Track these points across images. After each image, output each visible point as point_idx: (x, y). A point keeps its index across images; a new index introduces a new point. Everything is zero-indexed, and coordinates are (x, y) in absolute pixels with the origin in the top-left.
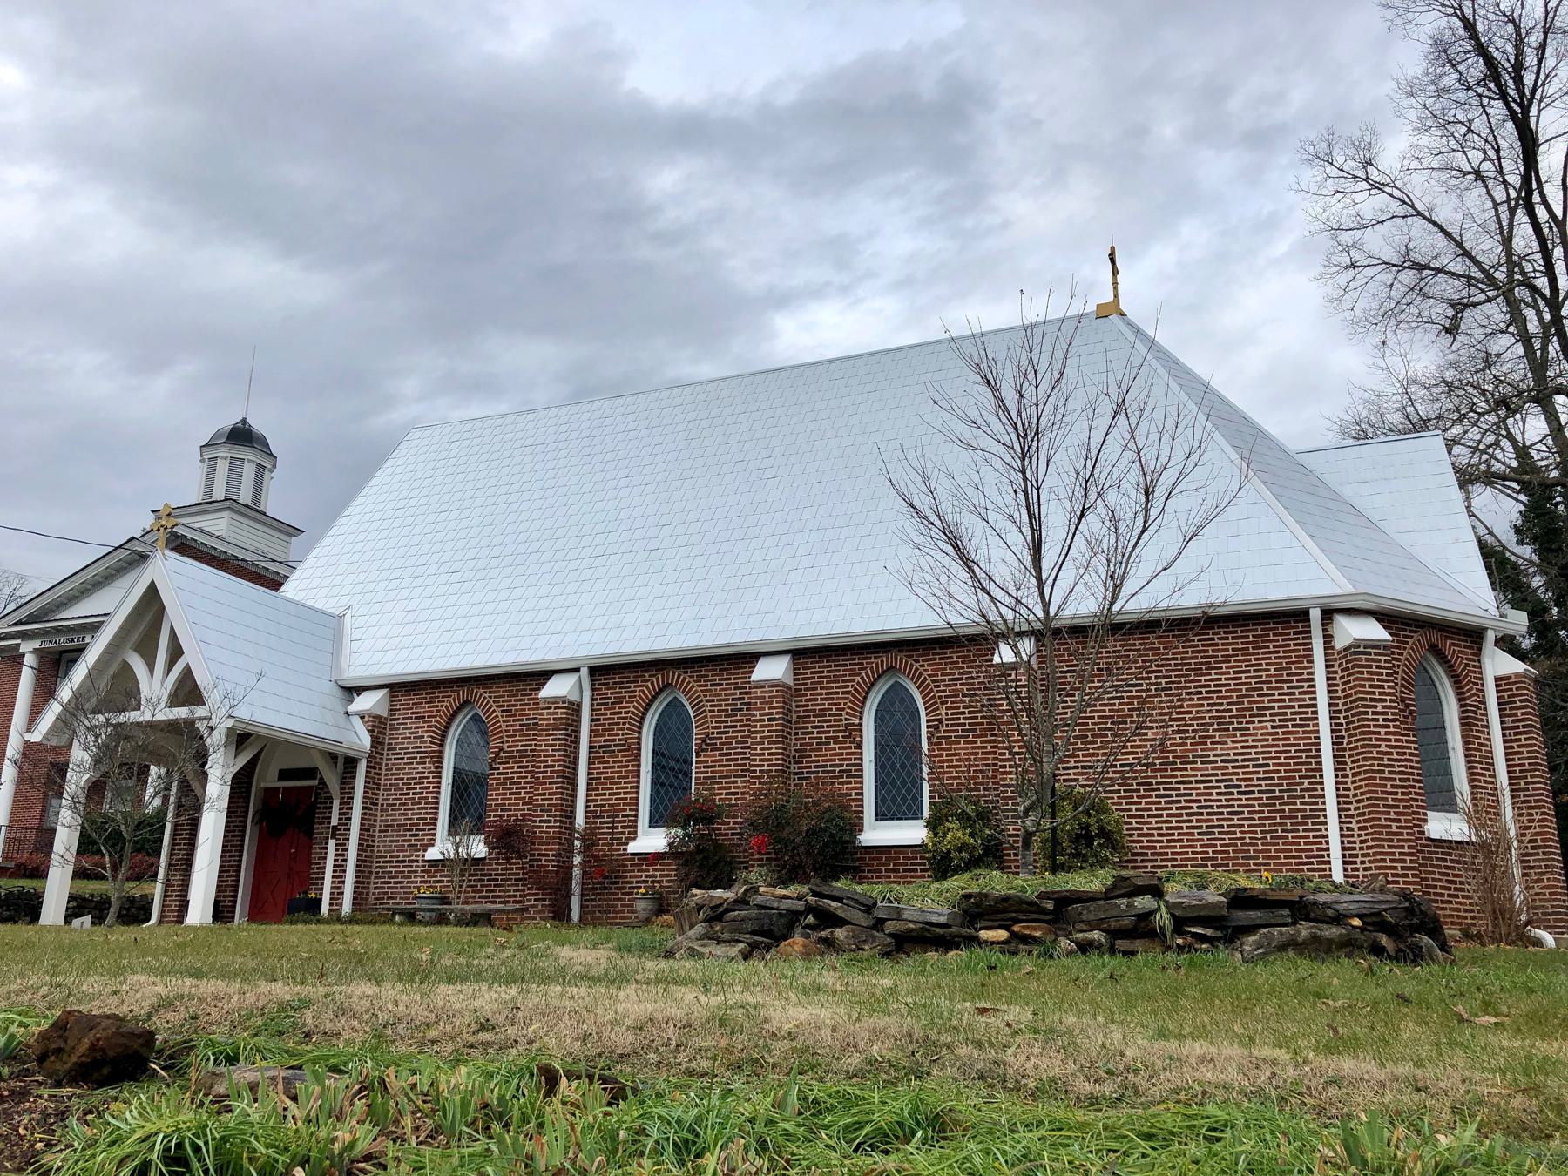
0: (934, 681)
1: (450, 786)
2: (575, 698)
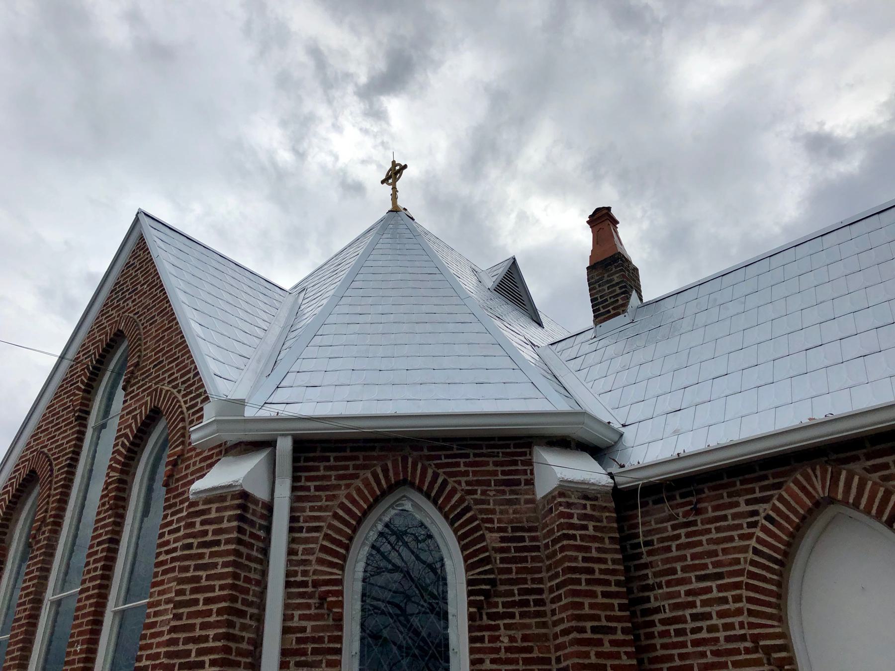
0: (481, 511)
2: (260, 493)
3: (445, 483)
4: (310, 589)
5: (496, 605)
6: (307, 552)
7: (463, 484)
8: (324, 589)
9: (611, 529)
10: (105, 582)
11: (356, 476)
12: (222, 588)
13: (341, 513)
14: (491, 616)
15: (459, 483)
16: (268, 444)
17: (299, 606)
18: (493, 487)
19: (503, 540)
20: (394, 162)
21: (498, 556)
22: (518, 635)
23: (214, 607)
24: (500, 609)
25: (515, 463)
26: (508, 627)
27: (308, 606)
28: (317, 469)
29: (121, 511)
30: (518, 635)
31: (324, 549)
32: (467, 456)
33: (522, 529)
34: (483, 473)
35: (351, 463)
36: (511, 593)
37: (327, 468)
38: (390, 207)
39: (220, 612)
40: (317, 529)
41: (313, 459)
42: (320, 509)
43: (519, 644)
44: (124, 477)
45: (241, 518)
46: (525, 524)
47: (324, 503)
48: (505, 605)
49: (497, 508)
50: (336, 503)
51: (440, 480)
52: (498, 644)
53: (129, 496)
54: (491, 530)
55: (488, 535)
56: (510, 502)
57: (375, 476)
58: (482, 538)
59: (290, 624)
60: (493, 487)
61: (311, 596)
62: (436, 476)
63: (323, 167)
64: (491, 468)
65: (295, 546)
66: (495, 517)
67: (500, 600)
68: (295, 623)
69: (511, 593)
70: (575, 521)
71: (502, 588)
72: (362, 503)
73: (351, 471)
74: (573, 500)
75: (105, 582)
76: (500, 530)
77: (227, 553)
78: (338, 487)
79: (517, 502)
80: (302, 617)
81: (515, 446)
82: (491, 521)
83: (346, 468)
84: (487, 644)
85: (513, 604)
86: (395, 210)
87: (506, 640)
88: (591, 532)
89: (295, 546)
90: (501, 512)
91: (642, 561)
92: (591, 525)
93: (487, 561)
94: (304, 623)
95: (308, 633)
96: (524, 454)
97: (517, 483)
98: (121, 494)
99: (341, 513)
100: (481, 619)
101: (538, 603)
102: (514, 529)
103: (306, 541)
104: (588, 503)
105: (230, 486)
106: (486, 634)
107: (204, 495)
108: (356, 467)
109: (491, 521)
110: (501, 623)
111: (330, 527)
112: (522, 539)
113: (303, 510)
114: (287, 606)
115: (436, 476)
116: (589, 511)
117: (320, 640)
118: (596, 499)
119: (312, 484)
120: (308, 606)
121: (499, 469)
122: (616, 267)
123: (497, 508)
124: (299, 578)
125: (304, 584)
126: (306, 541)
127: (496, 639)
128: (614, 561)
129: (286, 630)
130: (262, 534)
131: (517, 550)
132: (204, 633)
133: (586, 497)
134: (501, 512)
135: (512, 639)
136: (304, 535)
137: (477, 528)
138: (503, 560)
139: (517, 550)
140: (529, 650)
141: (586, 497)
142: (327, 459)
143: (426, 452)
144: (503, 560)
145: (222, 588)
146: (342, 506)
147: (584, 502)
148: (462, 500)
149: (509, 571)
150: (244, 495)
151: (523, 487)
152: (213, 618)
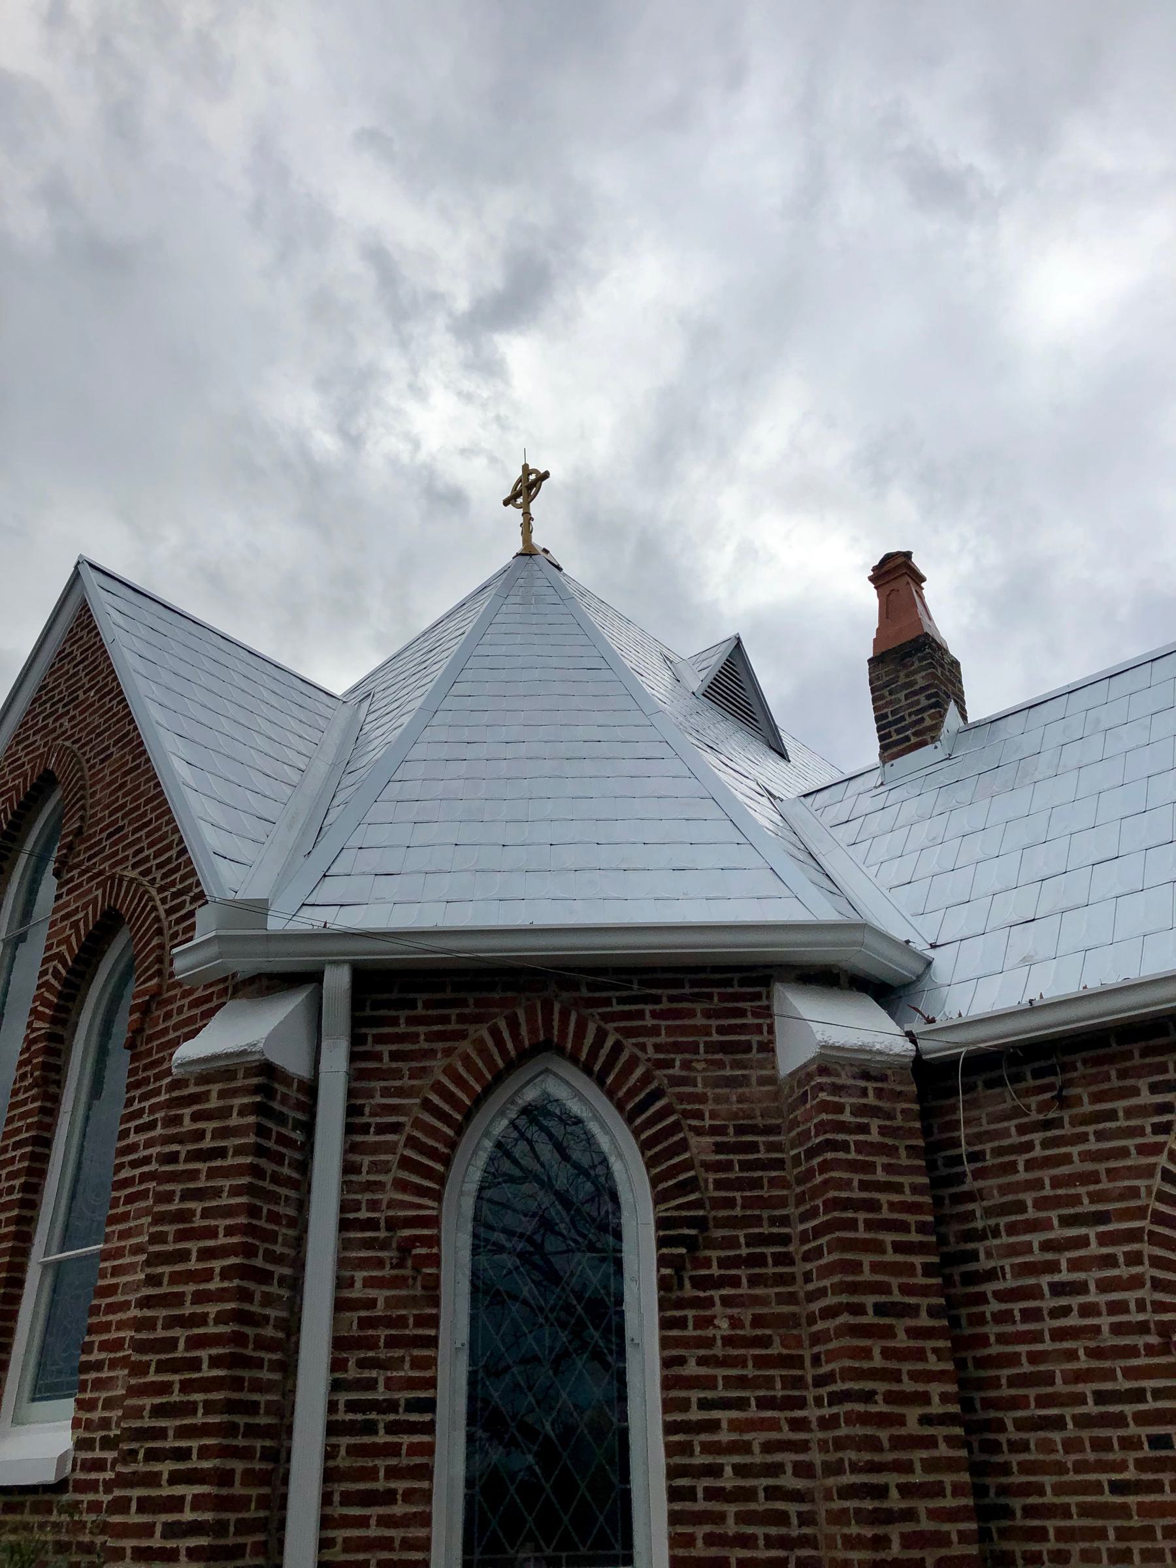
0: (681, 1098)
1: (464, 1358)
2: (295, 1063)
3: (617, 1048)
4: (382, 1234)
5: (707, 1263)
6: (375, 1167)
7: (650, 1050)
8: (407, 1232)
9: (911, 1133)
10: (27, 1213)
11: (461, 1035)
12: (229, 1231)
13: (436, 1099)
14: (698, 1282)
15: (643, 1047)
16: (311, 978)
17: (362, 1263)
18: (702, 1054)
19: (719, 1148)
20: (525, 467)
21: (711, 1177)
22: (747, 1315)
23: (217, 1265)
24: (715, 1271)
25: (742, 1013)
26: (727, 1301)
27: (380, 1264)
28: (394, 1022)
29: (53, 1089)
30: (747, 1315)
31: (405, 1163)
32: (657, 1000)
33: (754, 1130)
34: (684, 1030)
35: (453, 1012)
36: (732, 1243)
37: (411, 1021)
38: (519, 547)
39: (226, 1274)
40: (396, 1128)
41: (388, 1004)
42: (401, 1092)
43: (748, 1332)
44: (59, 1030)
45: (259, 1109)
46: (759, 1121)
47: (406, 1082)
48: (723, 1263)
49: (710, 1093)
50: (429, 1081)
51: (609, 1043)
52: (710, 1332)
53: (67, 1062)
54: (698, 1131)
55: (693, 1140)
56: (731, 1082)
57: (495, 1033)
58: (683, 1146)
59: (347, 1294)
60: (702, 1054)
61: (384, 1245)
62: (601, 1036)
63: (393, 461)
64: (700, 1021)
65: (357, 1158)
66: (706, 1108)
67: (714, 1254)
68: (358, 1292)
69: (732, 1243)
70: (847, 1117)
71: (718, 1233)
72: (472, 1082)
73: (453, 1026)
74: (844, 1080)
75: (27, 1213)
76: (715, 1131)
77: (239, 1170)
78: (429, 1054)
79: (743, 1081)
80: (369, 1283)
81: (743, 983)
82: (699, 1115)
83: (445, 1020)
84: (690, 1332)
85: (736, 1262)
86: (528, 552)
87: (724, 1324)
88: (874, 1137)
89: (357, 1158)
90: (718, 1099)
91: (965, 1188)
92: (875, 1124)
93: (690, 1185)
94: (372, 1293)
95: (379, 1312)
96: (757, 997)
97: (747, 1047)
98: (52, 1060)
99: (436, 1099)
100: (681, 1286)
101: (781, 1259)
102: (740, 1130)
103: (376, 1148)
104: (870, 1085)
105: (243, 1053)
106: (690, 1313)
107: (197, 1069)
108: (462, 1019)
109: (699, 1115)
110: (716, 1294)
111: (418, 1124)
112: (753, 1147)
113: (370, 1094)
114: (342, 1263)
115: (601, 1036)
116: (871, 1100)
117: (401, 1322)
118: (883, 1078)
119: (385, 1049)
120: (380, 1264)
121: (714, 1023)
122: (920, 660)
123: (710, 1093)
124: (363, 1214)
125: (372, 1224)
126: (376, 1148)
127: (708, 1322)
128: (915, 1189)
129: (341, 1305)
130: (298, 1136)
131: (745, 1166)
132: (199, 1309)
133: (866, 1076)
134: (718, 1099)
135: (735, 1323)
136: (372, 1138)
137: (675, 1127)
138: (719, 1185)
139: (745, 1165)
140: (765, 1342)
141: (866, 1076)
142: (412, 1005)
143: (585, 993)
144: (719, 1185)
145: (229, 1231)
146: (439, 1088)
147: (862, 1083)
148: (646, 1078)
149: (730, 1203)
150: (268, 1069)
151: (754, 1055)
152: (214, 1285)
